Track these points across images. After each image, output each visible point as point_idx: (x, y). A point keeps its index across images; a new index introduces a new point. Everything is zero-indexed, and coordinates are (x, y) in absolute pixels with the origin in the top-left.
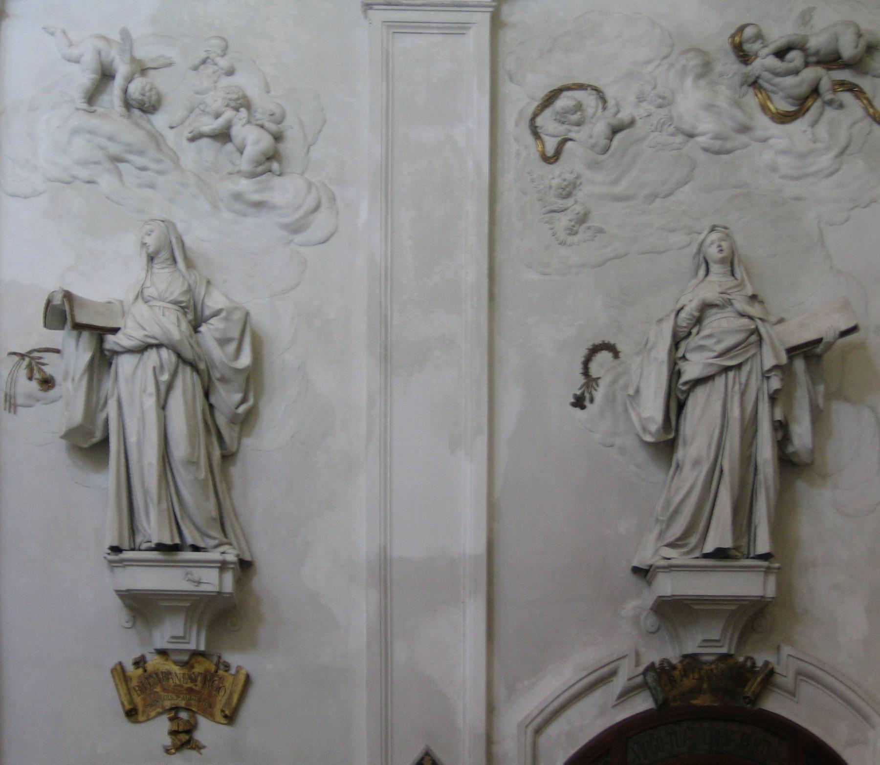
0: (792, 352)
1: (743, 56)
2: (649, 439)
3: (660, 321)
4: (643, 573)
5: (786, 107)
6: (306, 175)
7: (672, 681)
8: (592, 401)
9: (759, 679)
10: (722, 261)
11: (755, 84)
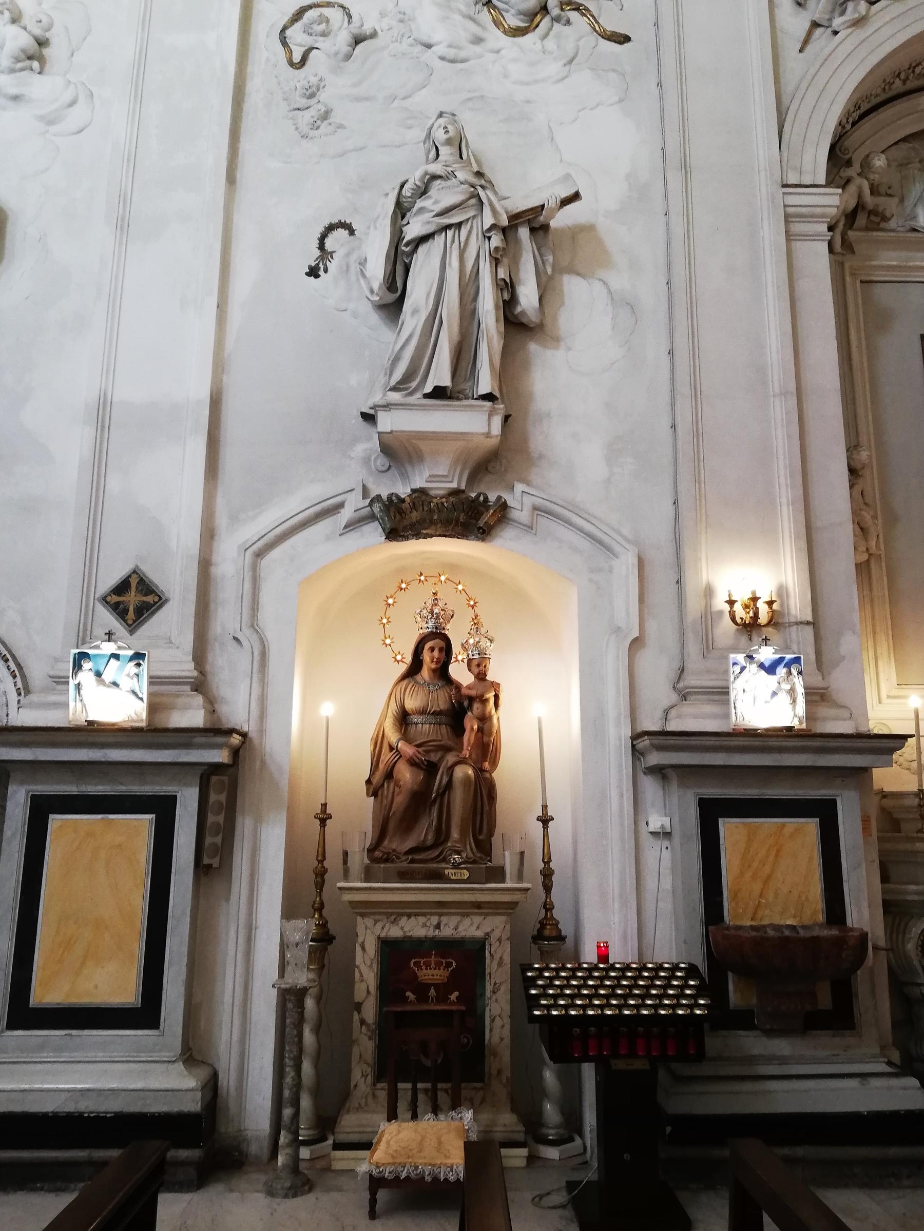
4: (370, 418)
5: (513, 21)
6: (68, 76)
7: (401, 512)
8: (326, 271)
10: (449, 142)
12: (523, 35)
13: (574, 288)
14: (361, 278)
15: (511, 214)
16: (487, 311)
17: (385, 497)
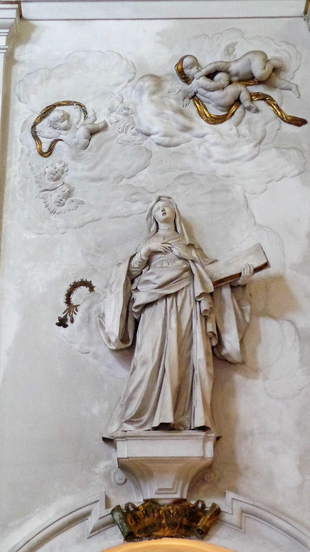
0: (218, 283)
1: (186, 79)
2: (114, 348)
3: (119, 264)
4: (109, 441)
5: (216, 112)
7: (136, 518)
8: (72, 321)
9: (208, 516)
10: (166, 221)
11: (194, 97)
12: (222, 122)
13: (269, 328)
14: (100, 329)
15: (215, 280)
16: (199, 360)
17: (123, 507)
